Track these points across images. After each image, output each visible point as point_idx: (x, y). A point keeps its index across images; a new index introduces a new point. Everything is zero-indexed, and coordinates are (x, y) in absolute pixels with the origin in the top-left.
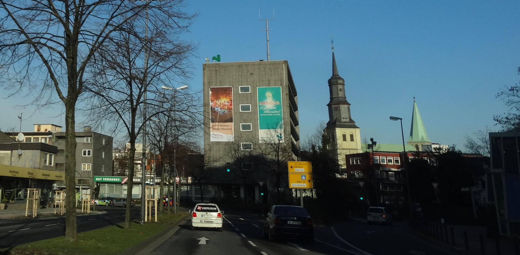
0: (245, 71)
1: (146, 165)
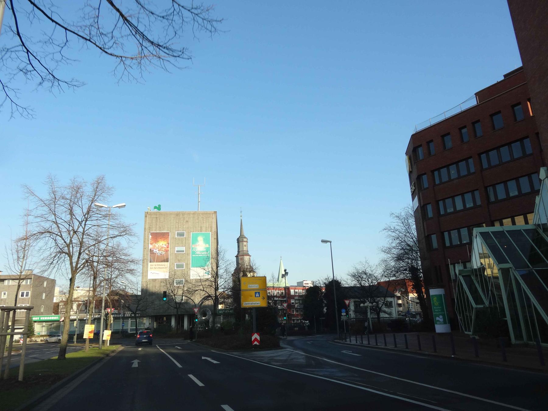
1: (112, 322)
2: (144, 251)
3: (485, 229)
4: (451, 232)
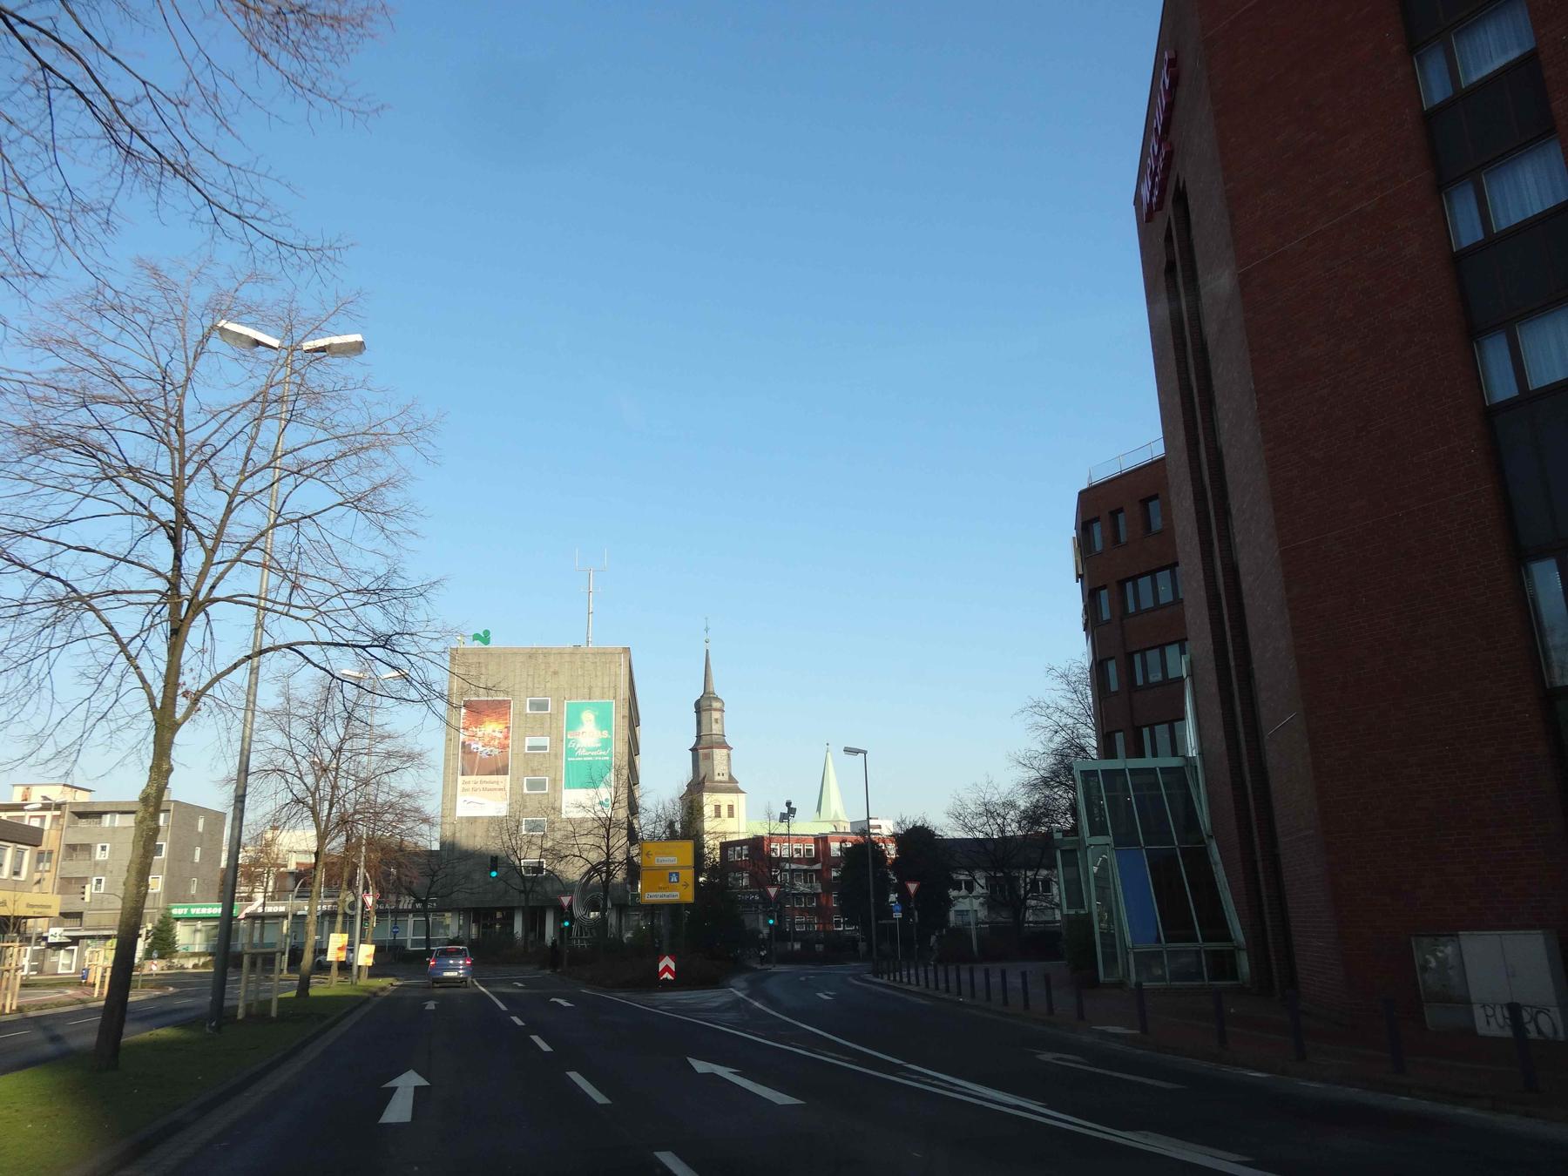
2: (447, 747)
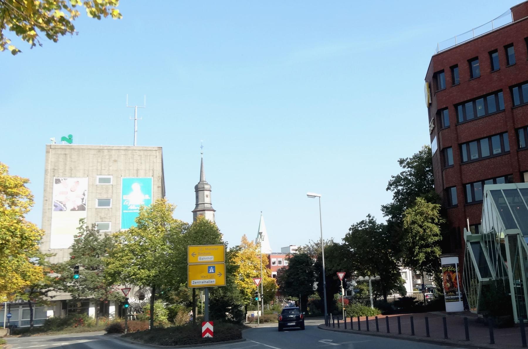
0: (107, 157)
3: (502, 186)
4: (474, 184)
